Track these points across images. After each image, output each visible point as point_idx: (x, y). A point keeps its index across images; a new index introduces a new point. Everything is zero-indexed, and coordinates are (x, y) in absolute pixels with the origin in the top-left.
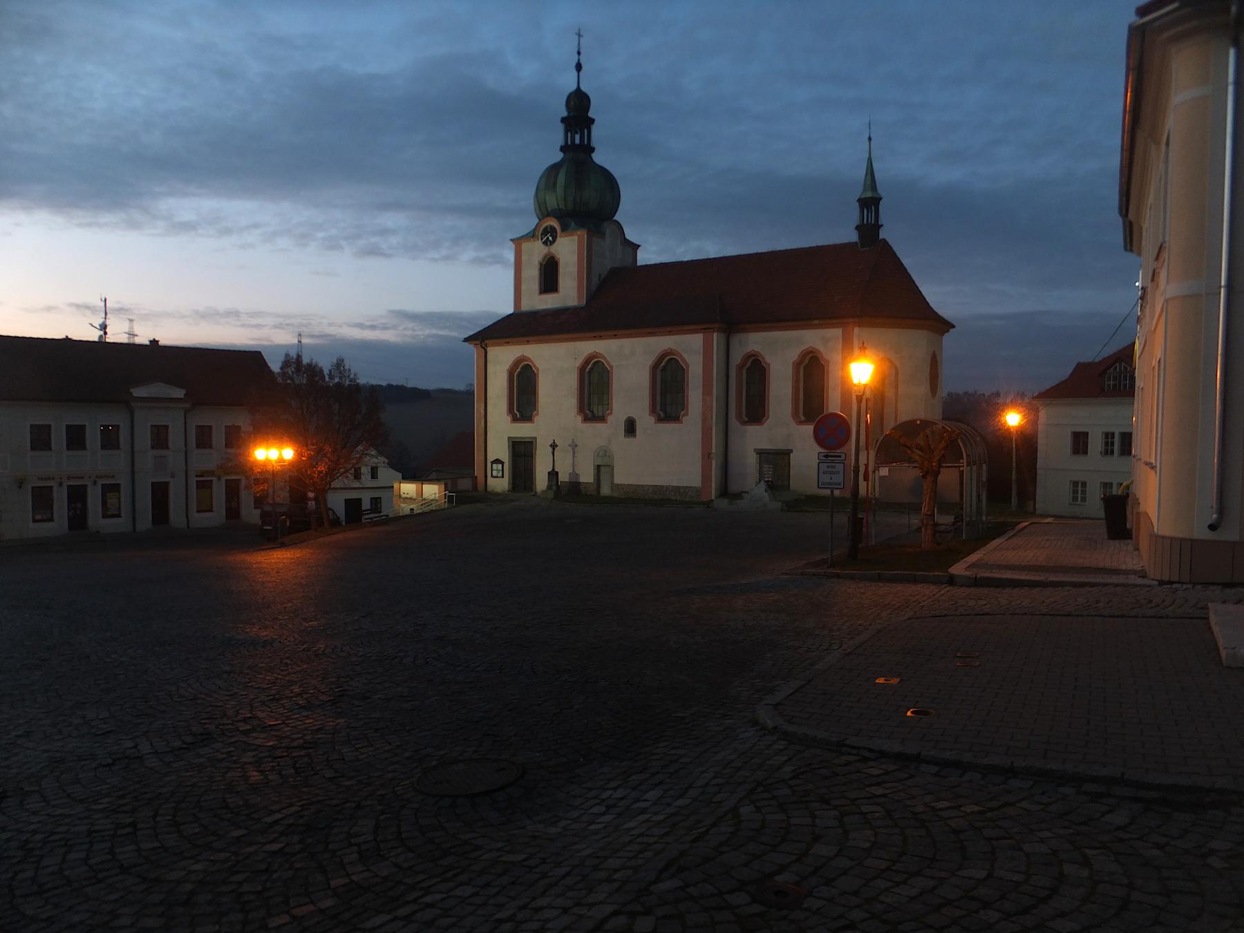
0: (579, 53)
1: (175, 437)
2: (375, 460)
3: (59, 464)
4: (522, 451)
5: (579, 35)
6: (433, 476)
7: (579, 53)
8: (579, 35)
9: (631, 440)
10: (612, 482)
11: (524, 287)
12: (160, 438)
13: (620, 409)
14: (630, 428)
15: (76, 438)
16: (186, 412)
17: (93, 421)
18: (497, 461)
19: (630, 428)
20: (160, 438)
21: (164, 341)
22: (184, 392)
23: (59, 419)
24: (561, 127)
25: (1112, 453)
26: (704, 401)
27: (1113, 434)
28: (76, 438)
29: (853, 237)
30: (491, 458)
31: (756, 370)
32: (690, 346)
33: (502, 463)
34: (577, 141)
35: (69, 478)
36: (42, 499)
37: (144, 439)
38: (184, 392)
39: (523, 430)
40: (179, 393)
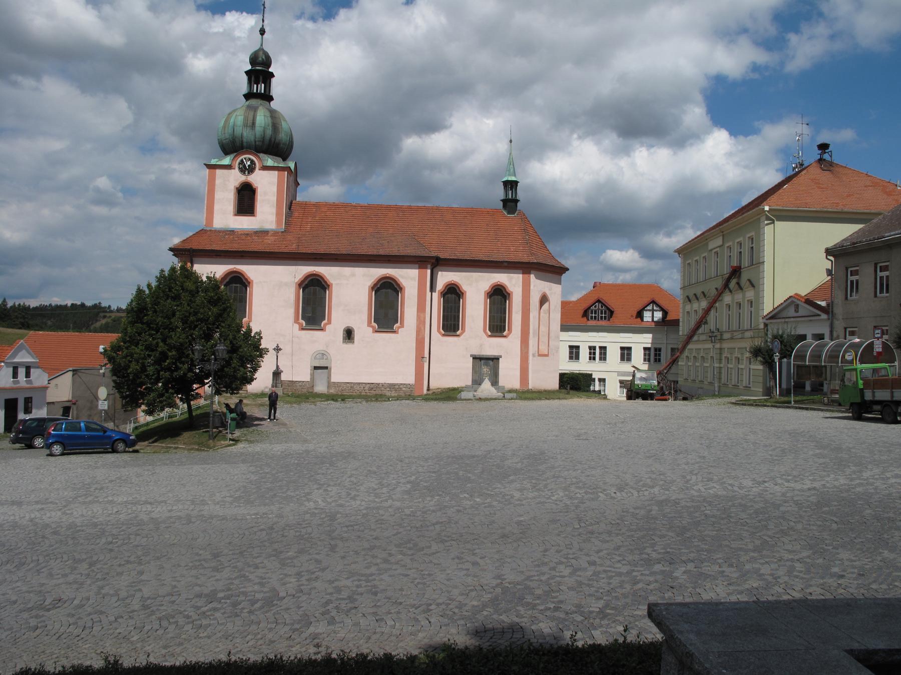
9: (350, 346)
11: (217, 207)
14: (349, 334)
19: (349, 334)
24: (245, 78)
25: (594, 359)
26: (418, 317)
27: (594, 348)
32: (408, 278)
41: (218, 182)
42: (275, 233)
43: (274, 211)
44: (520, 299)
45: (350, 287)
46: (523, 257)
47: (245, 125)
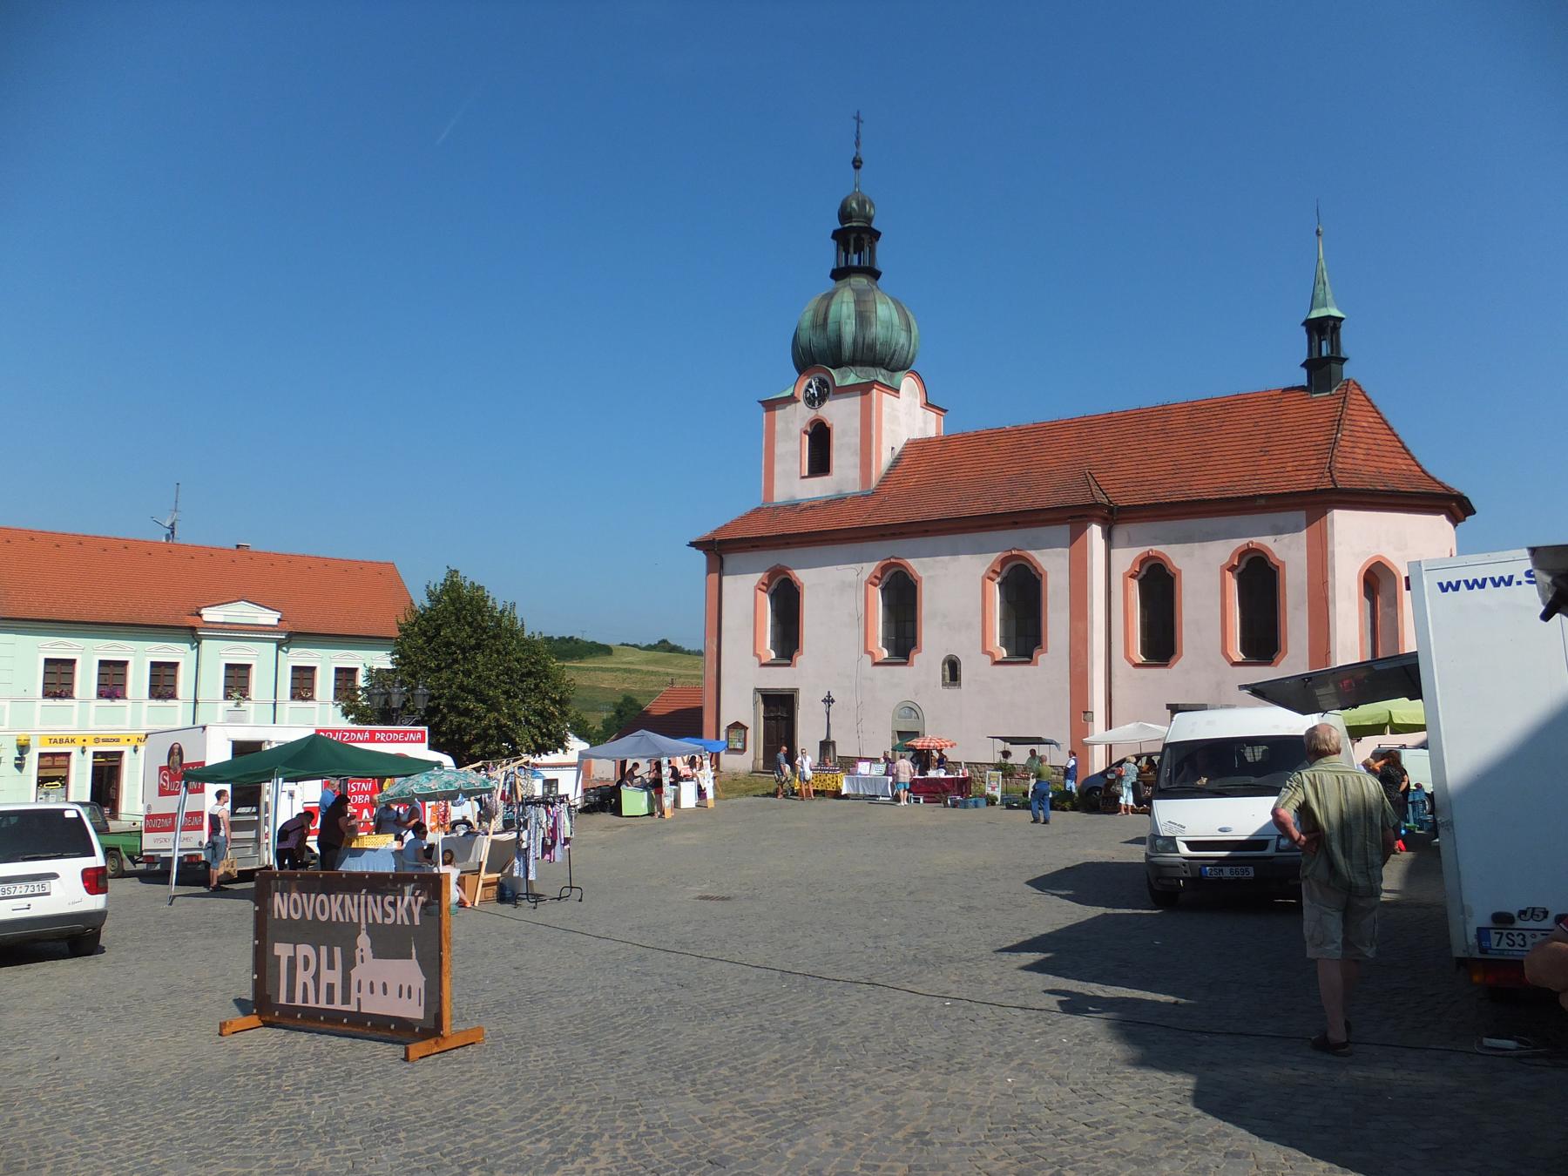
0: (857, 144)
1: (259, 683)
2: (948, 1155)
3: (85, 721)
4: (779, 709)
5: (858, 120)
6: (13, 820)
7: (857, 144)
8: (858, 120)
10: (861, 759)
11: (778, 468)
12: (237, 679)
13: (934, 641)
14: (953, 670)
15: (112, 680)
16: (279, 648)
17: (139, 656)
18: (737, 726)
19: (953, 670)
20: (237, 679)
21: (256, 545)
22: (278, 615)
23: (88, 653)
28: (112, 680)
29: (1301, 378)
30: (726, 721)
31: (1158, 587)
33: (746, 728)
34: (855, 263)
35: (97, 741)
36: (53, 771)
37: (215, 680)
38: (278, 615)
39: (779, 679)
40: (270, 618)
41: (779, 426)
42: (855, 497)
43: (857, 460)
44: (1304, 577)
45: (958, 588)
46: (1306, 481)
47: (814, 326)
